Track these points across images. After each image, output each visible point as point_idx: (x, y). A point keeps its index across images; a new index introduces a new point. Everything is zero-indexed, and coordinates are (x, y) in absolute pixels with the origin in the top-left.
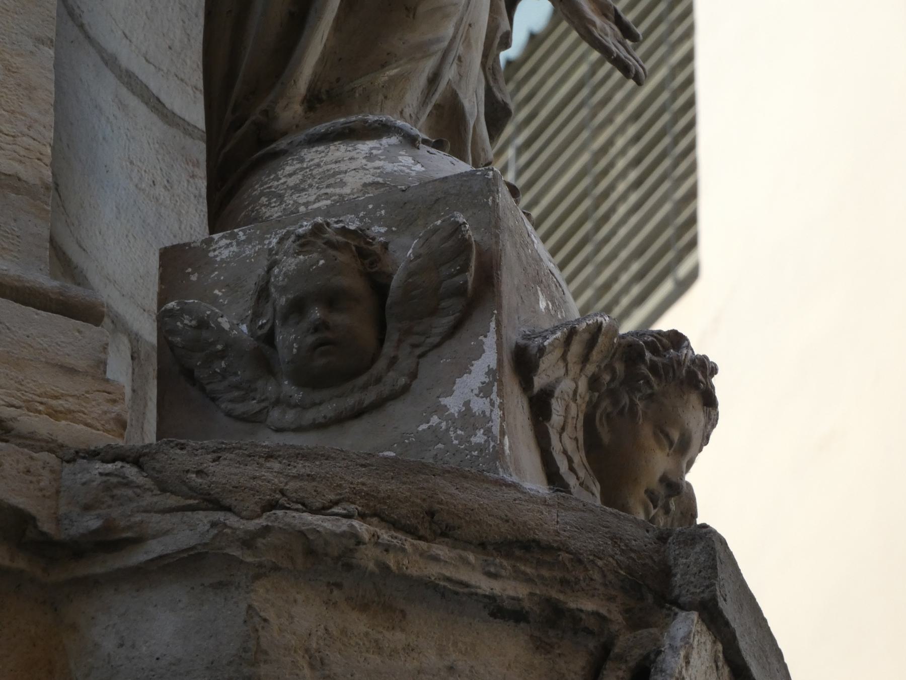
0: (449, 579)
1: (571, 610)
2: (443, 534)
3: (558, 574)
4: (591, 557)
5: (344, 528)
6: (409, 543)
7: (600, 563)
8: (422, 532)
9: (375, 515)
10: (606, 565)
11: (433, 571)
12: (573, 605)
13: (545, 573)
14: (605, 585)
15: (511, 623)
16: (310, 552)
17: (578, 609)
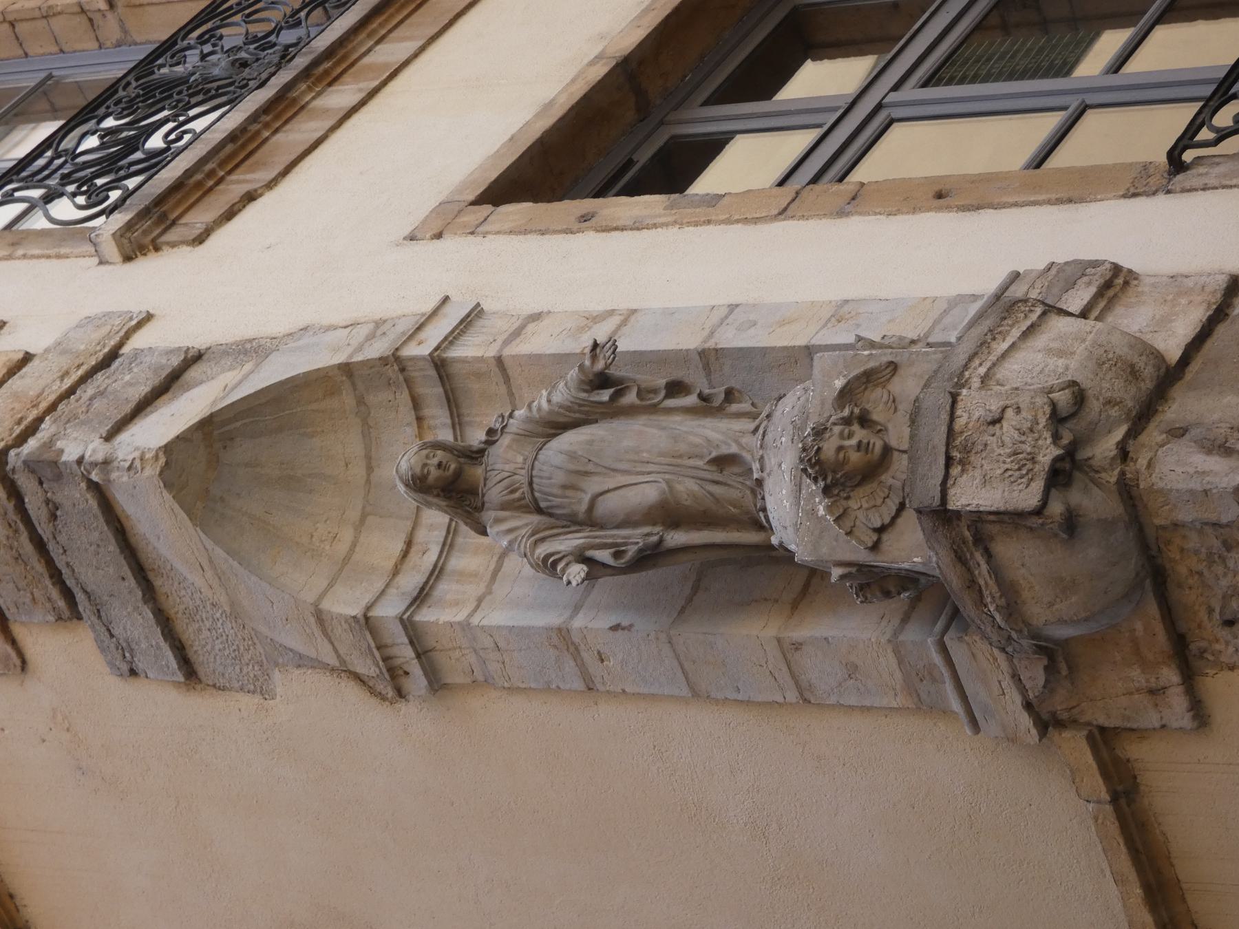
6: (986, 593)
11: (991, 583)
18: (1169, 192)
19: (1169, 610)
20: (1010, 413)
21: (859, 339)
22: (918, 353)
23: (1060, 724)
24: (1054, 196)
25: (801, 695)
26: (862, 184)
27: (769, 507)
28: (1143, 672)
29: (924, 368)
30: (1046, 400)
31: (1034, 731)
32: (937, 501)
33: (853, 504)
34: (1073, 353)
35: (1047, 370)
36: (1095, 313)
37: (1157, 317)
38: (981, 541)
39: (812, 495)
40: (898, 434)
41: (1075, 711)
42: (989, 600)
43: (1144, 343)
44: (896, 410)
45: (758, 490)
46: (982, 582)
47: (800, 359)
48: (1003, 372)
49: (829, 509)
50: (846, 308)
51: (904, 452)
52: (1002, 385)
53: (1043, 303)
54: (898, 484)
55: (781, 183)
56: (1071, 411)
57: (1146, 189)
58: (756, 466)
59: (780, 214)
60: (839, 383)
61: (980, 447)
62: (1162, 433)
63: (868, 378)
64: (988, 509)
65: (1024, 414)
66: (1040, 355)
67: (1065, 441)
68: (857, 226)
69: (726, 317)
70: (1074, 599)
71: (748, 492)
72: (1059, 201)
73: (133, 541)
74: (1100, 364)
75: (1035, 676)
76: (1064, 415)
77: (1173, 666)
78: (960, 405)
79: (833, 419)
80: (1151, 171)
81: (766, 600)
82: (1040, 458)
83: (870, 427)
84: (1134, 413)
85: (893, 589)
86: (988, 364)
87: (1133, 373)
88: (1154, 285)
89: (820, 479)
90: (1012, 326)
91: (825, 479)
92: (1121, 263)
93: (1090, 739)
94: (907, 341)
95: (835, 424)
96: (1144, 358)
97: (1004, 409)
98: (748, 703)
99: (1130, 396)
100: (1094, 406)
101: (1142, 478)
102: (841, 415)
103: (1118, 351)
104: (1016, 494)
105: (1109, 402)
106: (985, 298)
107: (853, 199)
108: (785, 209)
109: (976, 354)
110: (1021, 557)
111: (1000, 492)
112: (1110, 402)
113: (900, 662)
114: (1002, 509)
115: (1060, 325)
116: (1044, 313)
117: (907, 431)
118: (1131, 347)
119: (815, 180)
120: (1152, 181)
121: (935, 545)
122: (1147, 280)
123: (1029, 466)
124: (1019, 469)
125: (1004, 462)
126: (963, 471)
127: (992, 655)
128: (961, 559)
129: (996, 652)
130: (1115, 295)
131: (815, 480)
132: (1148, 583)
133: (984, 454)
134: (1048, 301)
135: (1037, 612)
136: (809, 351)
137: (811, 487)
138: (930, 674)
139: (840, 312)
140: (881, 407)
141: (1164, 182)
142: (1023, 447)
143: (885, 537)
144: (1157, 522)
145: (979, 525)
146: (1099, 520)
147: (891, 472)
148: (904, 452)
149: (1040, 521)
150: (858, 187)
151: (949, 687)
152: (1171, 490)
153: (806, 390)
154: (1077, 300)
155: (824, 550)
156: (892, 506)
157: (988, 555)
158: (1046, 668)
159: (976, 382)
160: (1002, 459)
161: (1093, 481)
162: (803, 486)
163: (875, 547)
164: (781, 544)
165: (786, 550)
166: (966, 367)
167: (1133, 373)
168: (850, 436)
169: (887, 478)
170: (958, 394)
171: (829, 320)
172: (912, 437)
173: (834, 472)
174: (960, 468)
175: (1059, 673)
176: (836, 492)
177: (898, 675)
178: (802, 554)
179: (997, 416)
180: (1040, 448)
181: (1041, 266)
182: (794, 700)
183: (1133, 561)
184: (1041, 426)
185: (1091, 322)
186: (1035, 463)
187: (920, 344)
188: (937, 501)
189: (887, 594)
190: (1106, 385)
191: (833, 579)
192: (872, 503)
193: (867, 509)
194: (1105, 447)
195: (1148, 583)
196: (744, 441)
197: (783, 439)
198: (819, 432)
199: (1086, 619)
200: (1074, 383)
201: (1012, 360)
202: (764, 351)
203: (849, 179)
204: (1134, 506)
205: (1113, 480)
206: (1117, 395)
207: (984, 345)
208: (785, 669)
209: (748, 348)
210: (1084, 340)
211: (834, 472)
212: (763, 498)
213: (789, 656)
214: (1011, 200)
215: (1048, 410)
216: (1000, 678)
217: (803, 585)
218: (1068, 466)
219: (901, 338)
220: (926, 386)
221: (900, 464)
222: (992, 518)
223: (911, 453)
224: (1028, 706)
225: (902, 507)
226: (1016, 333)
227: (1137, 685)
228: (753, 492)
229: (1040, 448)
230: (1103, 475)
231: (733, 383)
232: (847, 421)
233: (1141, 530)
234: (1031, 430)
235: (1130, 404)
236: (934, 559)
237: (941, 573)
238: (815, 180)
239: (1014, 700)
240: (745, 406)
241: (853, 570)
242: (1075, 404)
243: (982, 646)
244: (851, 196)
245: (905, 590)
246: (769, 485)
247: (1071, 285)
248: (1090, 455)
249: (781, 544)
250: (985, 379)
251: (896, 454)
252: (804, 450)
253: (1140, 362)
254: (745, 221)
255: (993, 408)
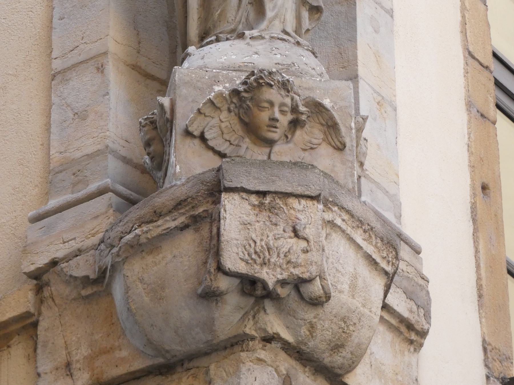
0: (164, 230)
1: (197, 215)
2: (161, 216)
3: (190, 206)
5: (134, 234)
6: (150, 226)
7: (199, 194)
8: (154, 219)
9: (142, 223)
11: (159, 231)
12: (197, 213)
13: (187, 208)
15: (187, 229)
16: (132, 247)
18: (488, 378)
19: (138, 378)
20: (303, 244)
21: (365, 119)
22: (353, 168)
23: (39, 289)
24: (484, 282)
25: (59, 72)
26: (494, 123)
27: (220, 44)
28: (85, 358)
29: (340, 173)
30: (314, 274)
31: (32, 268)
32: (228, 184)
33: (224, 115)
34: (353, 297)
35: (339, 275)
36: (387, 316)
37: (383, 368)
38: (195, 221)
39: (231, 80)
40: (283, 152)
41: (50, 301)
42: (145, 229)
43: (361, 356)
44: (305, 150)
45: (235, 35)
46: (160, 222)
47: (346, 69)
48: (337, 239)
49: (220, 95)
50: (389, 109)
51: (269, 157)
52: (326, 238)
53: (395, 273)
54: (242, 152)
55: (495, 56)
56: (305, 296)
57: (490, 360)
58: (255, 33)
59: (470, 53)
60: (327, 102)
61: (274, 220)
62: (287, 371)
63: (331, 127)
64: (222, 227)
65: (303, 256)
66: (352, 270)
67: (279, 290)
68: (459, 119)
69: (382, 7)
70: (147, 299)
71: (232, 27)
72: (480, 288)
74: (344, 320)
75: (81, 268)
76: (301, 289)
77: (90, 382)
78: (310, 203)
79: (297, 97)
80: (505, 364)
81: (139, 43)
82: (265, 269)
83: (290, 129)
84: (303, 347)
85: (152, 149)
86: (344, 226)
87: (337, 347)
88: (409, 365)
89: (245, 87)
90: (376, 246)
91: (245, 91)
92: (428, 337)
93: (27, 315)
94: (362, 160)
95: (292, 99)
96: (349, 356)
98: (50, 27)
99: (317, 345)
100: (309, 314)
101: (249, 354)
102: (300, 104)
103: (355, 334)
104: (235, 250)
105: (312, 327)
106: (397, 225)
107: (482, 115)
108: (473, 57)
109: (352, 216)
110: (182, 255)
111: (237, 237)
112: (312, 327)
113: (90, 156)
114: (222, 239)
116: (386, 273)
117: (286, 159)
118: (359, 345)
119: (498, 84)
120: (497, 364)
121: (189, 185)
122: (414, 359)
123: (259, 261)
124: (256, 252)
125: (262, 240)
126: (254, 206)
127: (97, 232)
128: (179, 205)
129: (100, 236)
130: (401, 333)
131: (245, 83)
132: (161, 360)
133: (268, 223)
134: (396, 278)
135: (135, 269)
136: (354, 78)
137: (237, 80)
138: (79, 182)
139: (386, 104)
140: (307, 138)
141: (496, 374)
142: (275, 256)
143: (197, 142)
144: (212, 367)
145: (209, 220)
146: (213, 319)
147: (251, 146)
148: (269, 157)
149: (212, 270)
150: (492, 119)
151: (68, 197)
152: (239, 378)
153: (321, 75)
154: (398, 301)
155: (184, 91)
156: (223, 148)
157: (184, 228)
158: (87, 277)
159: (328, 216)
160: (265, 238)
161: (246, 313)
162: (239, 73)
163: (188, 133)
164: (188, 55)
165: (184, 60)
166: (342, 208)
167: (337, 347)
168: (282, 112)
169: (247, 143)
171: (379, 95)
172: (282, 163)
173: (252, 99)
174: (256, 203)
175: (83, 289)
176: (235, 100)
177: (78, 154)
178: (181, 72)
179: (300, 234)
180: (274, 269)
181: (425, 272)
182: (54, 66)
183: (179, 348)
184: (292, 270)
185: (379, 312)
187: (359, 170)
188: (228, 184)
189: (148, 144)
190: (327, 324)
191: (159, 98)
192: (225, 131)
193: (220, 127)
194: (275, 323)
195: (161, 360)
196: (277, 22)
197: (279, 56)
198: (285, 86)
199: (129, 309)
200: (328, 297)
201: (347, 246)
202: (353, 40)
203: (498, 111)
204: (225, 348)
205: (247, 331)
206: (318, 333)
207: (360, 223)
208: (81, 58)
209: (355, 26)
210: (364, 306)
211: (252, 99)
212: (227, 39)
213: (92, 62)
214: (481, 247)
215: (306, 276)
216: (77, 239)
217: (154, 76)
219: (365, 154)
220: (325, 174)
221: (259, 154)
222: (215, 230)
223: (268, 163)
224: (54, 263)
225: (222, 155)
226: (370, 249)
227: (74, 353)
228: (233, 31)
229: (274, 269)
230: (251, 322)
231: (326, 14)
232: (295, 109)
233: (207, 354)
234: (289, 262)
235: (311, 344)
236: (179, 183)
237: (167, 189)
238: (498, 84)
239: (59, 251)
240: (306, 24)
241: (168, 115)
242: (311, 299)
243: (104, 223)
244: (484, 113)
245: (152, 159)
246: (239, 44)
247: (410, 296)
248: (268, 311)
249: (188, 55)
250: (331, 224)
251: (267, 150)
252: (270, 73)
253: (345, 353)
254: (464, 24)
255: (307, 231)
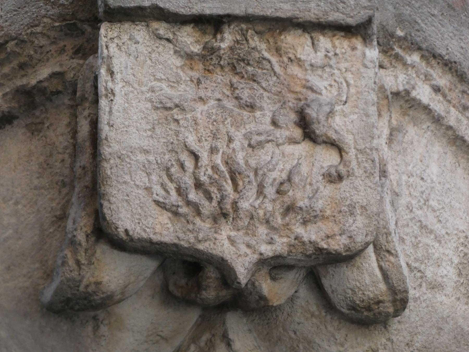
1: (34, 87)
3: (15, 63)
4: (29, 31)
7: (39, 29)
10: (44, 27)
12: (33, 82)
14: (53, 43)
17: (38, 82)
20: (327, 159)
30: (360, 239)
35: (428, 240)
52: (390, 140)
56: (336, 299)
61: (245, 95)
64: (104, 118)
65: (327, 191)
67: (266, 287)
73: (336, 148)
76: (326, 282)
78: (342, 44)
82: (226, 230)
86: (438, 106)
97: (336, 145)
104: (141, 179)
111: (145, 144)
114: (106, 150)
115: (318, 132)
123: (208, 208)
124: (198, 185)
125: (213, 150)
126: (190, 57)
133: (229, 104)
142: (251, 192)
149: (81, 237)
159: (395, 79)
160: (221, 145)
170: (366, 39)
174: (196, 49)
179: (320, 130)
180: (250, 230)
184: (300, 230)
186: (215, 220)
200: (400, 302)
201: (449, 159)
215: (338, 244)
218: (211, 294)
222: (84, 128)
229: (250, 230)
242: (353, 308)
250: (403, 100)
255: (338, 121)
